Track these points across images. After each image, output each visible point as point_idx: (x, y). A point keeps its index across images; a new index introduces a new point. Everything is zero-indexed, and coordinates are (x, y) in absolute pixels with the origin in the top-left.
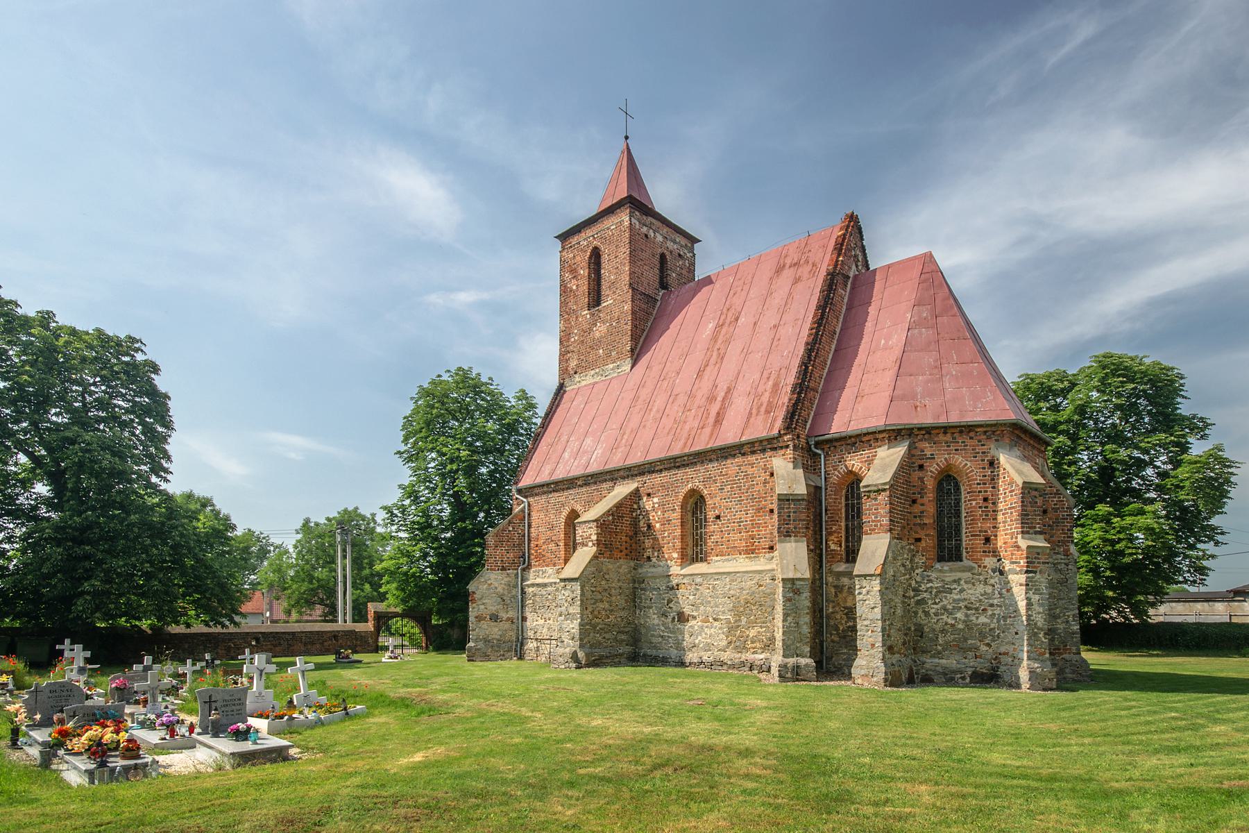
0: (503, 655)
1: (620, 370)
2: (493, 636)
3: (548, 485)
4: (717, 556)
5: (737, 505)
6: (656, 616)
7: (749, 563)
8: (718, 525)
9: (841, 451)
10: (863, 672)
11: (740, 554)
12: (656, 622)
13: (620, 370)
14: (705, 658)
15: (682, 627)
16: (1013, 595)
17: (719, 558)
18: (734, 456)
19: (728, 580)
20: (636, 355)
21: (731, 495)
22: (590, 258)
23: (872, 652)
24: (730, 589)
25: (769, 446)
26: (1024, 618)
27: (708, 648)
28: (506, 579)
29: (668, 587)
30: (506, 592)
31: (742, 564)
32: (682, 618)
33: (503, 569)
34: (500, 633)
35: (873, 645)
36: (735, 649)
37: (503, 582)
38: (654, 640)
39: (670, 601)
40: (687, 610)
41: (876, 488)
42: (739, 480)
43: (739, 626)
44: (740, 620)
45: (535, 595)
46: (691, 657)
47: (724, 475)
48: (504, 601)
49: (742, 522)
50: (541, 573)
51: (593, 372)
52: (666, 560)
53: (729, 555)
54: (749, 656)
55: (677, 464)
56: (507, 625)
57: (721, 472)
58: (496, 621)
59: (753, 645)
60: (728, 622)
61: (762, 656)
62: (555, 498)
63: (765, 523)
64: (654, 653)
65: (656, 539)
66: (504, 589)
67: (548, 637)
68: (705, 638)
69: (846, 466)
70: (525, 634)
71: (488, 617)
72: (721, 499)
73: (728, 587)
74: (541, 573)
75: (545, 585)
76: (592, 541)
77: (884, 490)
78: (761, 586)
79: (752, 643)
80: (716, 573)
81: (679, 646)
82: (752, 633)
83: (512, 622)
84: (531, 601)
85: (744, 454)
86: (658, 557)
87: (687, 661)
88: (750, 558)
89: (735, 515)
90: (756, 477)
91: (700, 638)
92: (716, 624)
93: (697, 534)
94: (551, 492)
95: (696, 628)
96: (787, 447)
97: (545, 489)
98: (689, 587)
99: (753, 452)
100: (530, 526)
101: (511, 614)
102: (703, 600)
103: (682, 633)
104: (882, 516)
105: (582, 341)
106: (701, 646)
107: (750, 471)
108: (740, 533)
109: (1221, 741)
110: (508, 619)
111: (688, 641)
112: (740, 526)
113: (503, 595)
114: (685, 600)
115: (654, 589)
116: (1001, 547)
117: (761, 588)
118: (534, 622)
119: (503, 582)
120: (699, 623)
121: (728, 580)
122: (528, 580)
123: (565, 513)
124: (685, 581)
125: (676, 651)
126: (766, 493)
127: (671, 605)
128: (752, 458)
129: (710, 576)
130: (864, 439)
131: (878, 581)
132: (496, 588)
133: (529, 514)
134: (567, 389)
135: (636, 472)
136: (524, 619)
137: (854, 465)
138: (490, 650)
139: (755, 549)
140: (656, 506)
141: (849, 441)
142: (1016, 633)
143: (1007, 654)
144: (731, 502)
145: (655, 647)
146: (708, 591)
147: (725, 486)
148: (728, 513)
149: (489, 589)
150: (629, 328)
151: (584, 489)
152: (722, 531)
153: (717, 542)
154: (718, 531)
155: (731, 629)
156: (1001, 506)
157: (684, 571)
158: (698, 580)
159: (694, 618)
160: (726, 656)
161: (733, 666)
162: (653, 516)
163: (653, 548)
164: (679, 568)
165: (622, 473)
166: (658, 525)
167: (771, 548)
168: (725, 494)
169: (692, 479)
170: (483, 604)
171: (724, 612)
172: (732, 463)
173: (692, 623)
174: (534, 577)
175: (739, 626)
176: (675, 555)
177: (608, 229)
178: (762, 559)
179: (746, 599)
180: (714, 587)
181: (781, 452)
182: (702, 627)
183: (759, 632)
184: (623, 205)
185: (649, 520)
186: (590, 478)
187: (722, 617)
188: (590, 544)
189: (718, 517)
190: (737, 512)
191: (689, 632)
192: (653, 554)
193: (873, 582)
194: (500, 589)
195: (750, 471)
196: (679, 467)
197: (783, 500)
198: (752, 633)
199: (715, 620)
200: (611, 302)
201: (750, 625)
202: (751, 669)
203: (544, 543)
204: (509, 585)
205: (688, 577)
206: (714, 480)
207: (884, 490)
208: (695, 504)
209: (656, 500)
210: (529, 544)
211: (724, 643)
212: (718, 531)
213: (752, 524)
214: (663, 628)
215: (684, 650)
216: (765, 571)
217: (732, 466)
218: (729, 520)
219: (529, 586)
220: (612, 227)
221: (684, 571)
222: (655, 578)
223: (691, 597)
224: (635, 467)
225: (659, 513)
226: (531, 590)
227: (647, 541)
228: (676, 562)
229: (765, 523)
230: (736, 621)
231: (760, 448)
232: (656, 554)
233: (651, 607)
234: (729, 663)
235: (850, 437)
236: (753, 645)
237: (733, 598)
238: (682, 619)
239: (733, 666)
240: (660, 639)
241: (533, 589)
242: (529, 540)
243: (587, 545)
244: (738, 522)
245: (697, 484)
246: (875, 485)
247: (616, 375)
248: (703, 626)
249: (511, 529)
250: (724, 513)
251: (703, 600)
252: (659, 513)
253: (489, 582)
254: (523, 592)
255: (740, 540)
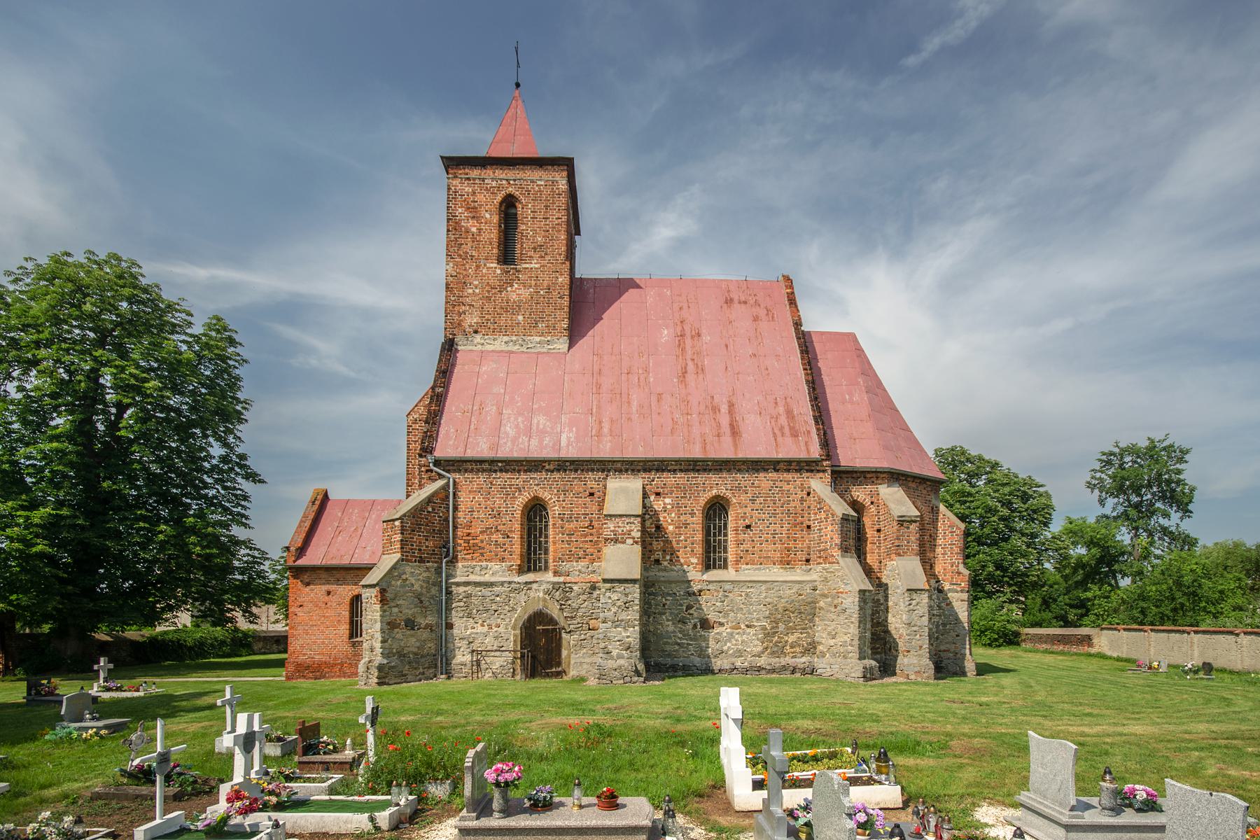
0: (423, 673)
1: (549, 347)
2: (410, 649)
3: (481, 462)
4: (747, 564)
5: (770, 517)
6: (670, 623)
7: (785, 573)
8: (749, 534)
9: (847, 482)
10: (916, 669)
11: (774, 564)
12: (671, 628)
13: (549, 347)
14: (738, 664)
15: (706, 634)
16: (953, 607)
17: (749, 566)
18: (766, 470)
19: (763, 588)
20: (575, 333)
21: (764, 507)
22: (501, 204)
23: (920, 652)
24: (766, 597)
25: (807, 468)
26: (966, 625)
27: (739, 654)
28: (425, 575)
29: (688, 592)
30: (424, 591)
31: (776, 573)
32: (705, 624)
33: (421, 561)
34: (418, 644)
35: (921, 647)
36: (771, 654)
37: (421, 577)
38: (668, 648)
39: (689, 607)
40: (712, 617)
41: (909, 519)
42: (773, 494)
43: (777, 632)
44: (777, 627)
45: (469, 596)
46: (717, 664)
47: (756, 487)
48: (421, 602)
49: (777, 534)
50: (478, 568)
51: (506, 339)
52: (682, 565)
53: (761, 564)
54: (786, 660)
55: (697, 468)
56: (425, 634)
57: (753, 484)
58: (413, 629)
59: (792, 650)
60: (764, 628)
61: (804, 659)
62: (519, 479)
63: (803, 537)
64: (669, 661)
65: (668, 542)
66: (422, 587)
67: (495, 648)
68: (736, 645)
69: (851, 496)
70: (449, 645)
71: (403, 623)
72: (752, 510)
73: (764, 595)
74: (478, 568)
75: (492, 584)
76: (633, 538)
77: (915, 522)
78: (800, 595)
79: (792, 647)
80: (750, 581)
81: (702, 653)
82: (791, 638)
83: (431, 630)
84: (462, 604)
85: (777, 471)
86: (671, 560)
87: (716, 668)
88: (786, 568)
89: (768, 527)
90: (792, 494)
91: (728, 644)
92: (748, 630)
93: (715, 541)
94: (495, 471)
95: (725, 634)
96: (824, 471)
97: (486, 466)
98: (715, 594)
99: (788, 471)
100: (456, 508)
101: (431, 619)
102: (733, 607)
103: (706, 639)
104: (913, 542)
105: (489, 298)
106: (731, 652)
107: (786, 487)
108: (775, 544)
109: (445, 707)
110: (427, 626)
111: (712, 647)
112: (774, 537)
113: (421, 594)
114: (709, 606)
115: (669, 595)
116: (939, 572)
117: (801, 597)
118: (462, 627)
119: (421, 577)
120: (728, 630)
121: (763, 588)
122: (454, 577)
123: (522, 499)
124: (710, 587)
125: (699, 659)
126: (803, 510)
127: (691, 612)
128: (789, 476)
129: (742, 584)
130: (868, 476)
131: (926, 595)
132: (413, 585)
133: (454, 494)
134: (459, 348)
135: (640, 468)
136: (450, 626)
137: (858, 496)
138: (407, 667)
139: (791, 561)
140: (669, 507)
141: (854, 475)
142: (957, 636)
143: (948, 651)
144: (764, 513)
145: (669, 655)
146: (740, 598)
147: (757, 497)
148: (761, 524)
149: (405, 586)
150: (567, 303)
151: (556, 475)
152: (753, 541)
153: (747, 551)
154: (749, 541)
155: (768, 635)
156: (940, 542)
157: (705, 577)
158: (728, 587)
159: (721, 624)
160: (763, 661)
161: (773, 671)
162: (665, 517)
163: (664, 551)
164: (700, 573)
165: (619, 465)
166: (671, 528)
167: (808, 561)
168: (756, 506)
169: (717, 485)
170: (397, 606)
171: (758, 620)
172: (765, 477)
173: (717, 630)
174: (462, 572)
175: (777, 632)
176: (694, 560)
177: (532, 181)
178: (798, 571)
179: (784, 607)
180: (747, 595)
181: (821, 475)
182: (732, 634)
183: (799, 638)
184: (559, 165)
185: (659, 520)
186: (568, 464)
187: (756, 624)
188: (630, 541)
189: (748, 527)
190: (771, 524)
191: (716, 639)
192: (664, 557)
193: (922, 596)
194: (417, 587)
195: (786, 487)
196: (698, 471)
197: (846, 520)
198: (791, 638)
199: (748, 626)
200: (536, 266)
201: (789, 631)
202: (793, 672)
203: (481, 532)
204: (428, 582)
205: (715, 584)
206: (744, 491)
207: (915, 522)
208: (716, 509)
209: (668, 501)
210: (454, 531)
211: (760, 649)
212: (749, 541)
213: (788, 537)
214: (680, 635)
215: (709, 657)
216: (804, 581)
217: (765, 480)
218: (761, 530)
219: (458, 584)
220: (539, 183)
221: (705, 577)
222: (670, 582)
223: (718, 604)
224: (639, 461)
225: (673, 515)
226: (461, 589)
227: (655, 543)
228: (695, 568)
229: (803, 537)
230: (773, 628)
231: (797, 468)
232: (668, 557)
233: (665, 614)
234: (768, 667)
235: (856, 472)
236: (792, 650)
237: (769, 606)
238: (705, 626)
239: (773, 671)
240: (677, 647)
241: (467, 589)
242: (455, 527)
243: (624, 542)
244: (772, 534)
245: (723, 491)
246: (909, 517)
247: (545, 350)
248: (733, 633)
249: (430, 509)
250: (756, 523)
251: (733, 607)
252: (673, 515)
253: (404, 577)
254: (449, 593)
255: (775, 551)
